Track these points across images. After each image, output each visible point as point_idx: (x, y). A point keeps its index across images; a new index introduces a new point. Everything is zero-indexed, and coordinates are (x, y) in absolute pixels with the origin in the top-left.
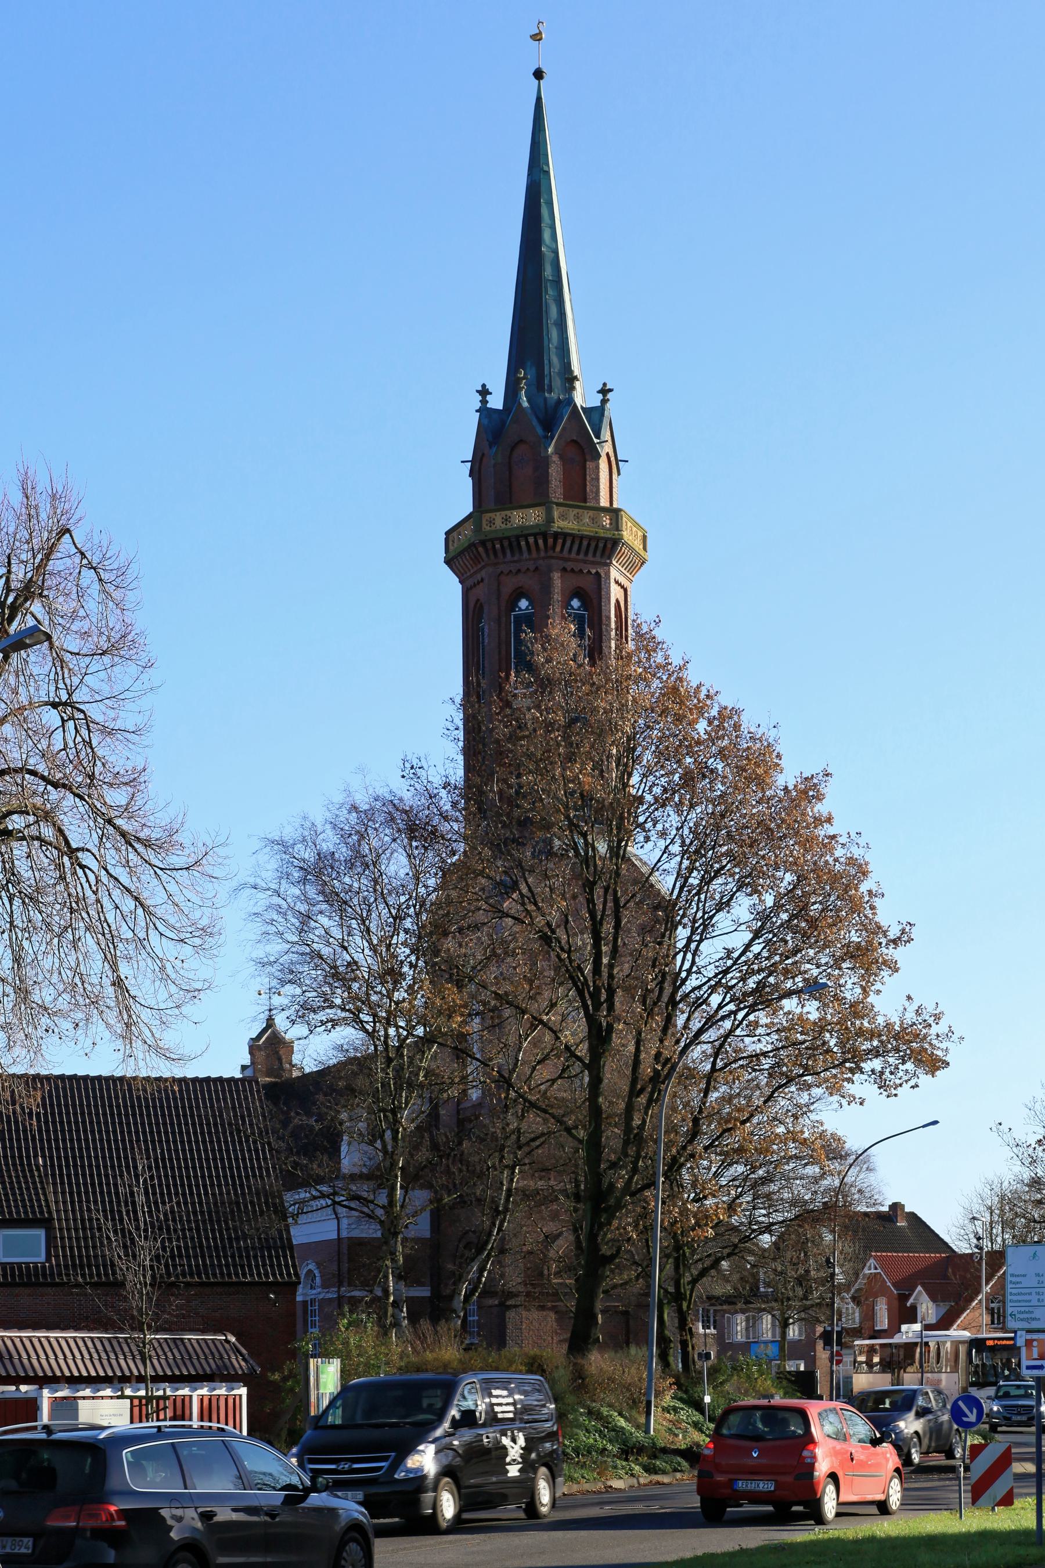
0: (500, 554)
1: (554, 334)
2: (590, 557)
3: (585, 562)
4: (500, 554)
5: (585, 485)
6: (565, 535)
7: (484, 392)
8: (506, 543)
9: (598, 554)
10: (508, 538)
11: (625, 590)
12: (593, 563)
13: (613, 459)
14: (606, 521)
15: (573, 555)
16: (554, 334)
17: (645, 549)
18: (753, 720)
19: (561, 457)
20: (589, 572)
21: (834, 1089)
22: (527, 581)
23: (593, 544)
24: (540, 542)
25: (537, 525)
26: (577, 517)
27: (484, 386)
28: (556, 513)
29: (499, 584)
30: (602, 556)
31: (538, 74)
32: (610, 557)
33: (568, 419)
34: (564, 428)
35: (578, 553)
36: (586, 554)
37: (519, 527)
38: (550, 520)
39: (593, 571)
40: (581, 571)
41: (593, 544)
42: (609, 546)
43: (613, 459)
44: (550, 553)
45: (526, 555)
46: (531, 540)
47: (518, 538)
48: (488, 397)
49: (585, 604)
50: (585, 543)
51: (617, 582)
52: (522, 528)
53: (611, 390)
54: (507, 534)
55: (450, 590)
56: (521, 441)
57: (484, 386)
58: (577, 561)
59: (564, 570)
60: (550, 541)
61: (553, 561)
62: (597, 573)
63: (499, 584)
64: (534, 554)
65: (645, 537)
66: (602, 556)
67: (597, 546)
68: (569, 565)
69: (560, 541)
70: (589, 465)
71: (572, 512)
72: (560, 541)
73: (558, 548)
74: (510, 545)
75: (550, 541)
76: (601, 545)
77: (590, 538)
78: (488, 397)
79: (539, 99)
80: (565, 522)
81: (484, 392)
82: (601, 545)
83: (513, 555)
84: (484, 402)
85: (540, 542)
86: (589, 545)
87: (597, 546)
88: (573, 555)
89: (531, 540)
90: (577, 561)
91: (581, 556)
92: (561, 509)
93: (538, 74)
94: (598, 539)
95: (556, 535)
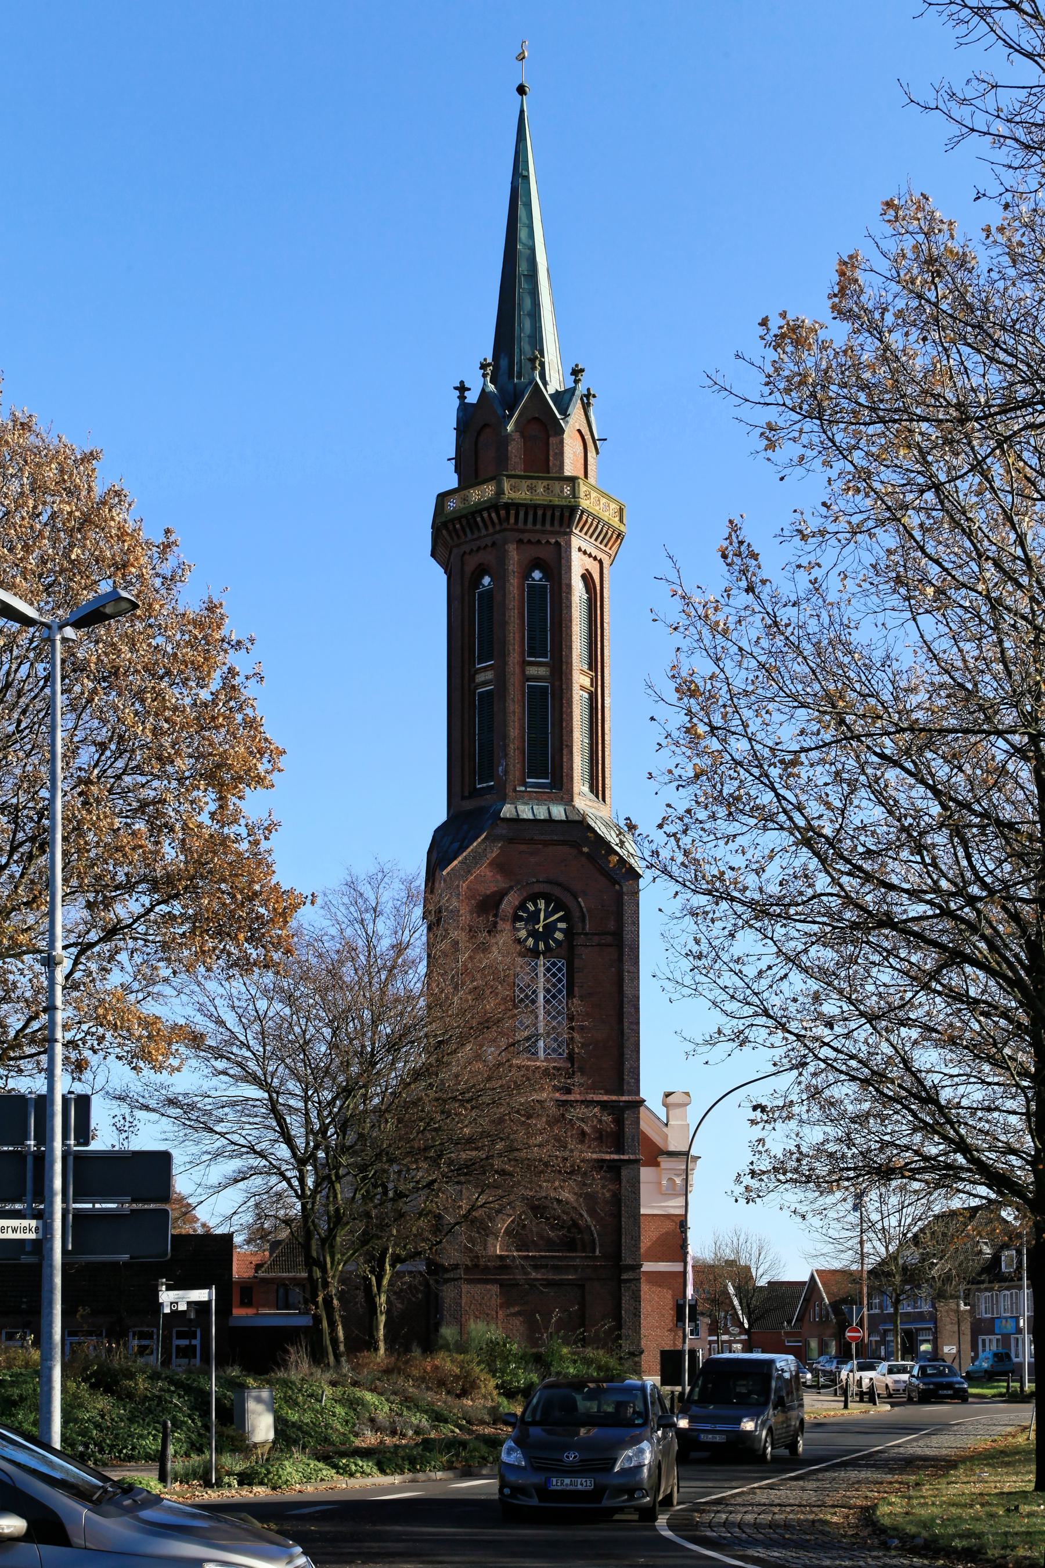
0: (461, 534)
1: (527, 324)
2: (548, 527)
3: (543, 532)
4: (461, 534)
5: (548, 460)
6: (516, 506)
7: (462, 389)
8: (464, 522)
9: (556, 523)
10: (465, 516)
11: (601, 562)
12: (552, 533)
13: (588, 437)
14: (567, 490)
15: (530, 526)
16: (527, 324)
17: (621, 521)
18: (143, 516)
19: (523, 436)
20: (548, 542)
21: (249, 1227)
22: (488, 557)
23: (549, 514)
24: (493, 515)
25: (490, 499)
26: (531, 489)
27: (462, 382)
28: (506, 486)
29: (463, 564)
30: (561, 525)
31: (521, 90)
32: (570, 526)
33: (530, 397)
34: (524, 406)
35: (535, 523)
36: (543, 523)
37: (476, 504)
38: (500, 492)
39: (553, 541)
40: (539, 542)
41: (549, 514)
42: (567, 514)
43: (588, 437)
44: (505, 525)
45: (484, 532)
46: (485, 515)
47: (473, 514)
48: (467, 394)
49: (547, 575)
50: (540, 513)
51: (580, 550)
52: (479, 503)
53: (582, 370)
54: (465, 512)
55: (437, 579)
56: (486, 425)
57: (462, 382)
58: (536, 531)
59: (520, 542)
60: (503, 513)
61: (508, 533)
62: (557, 543)
63: (463, 564)
64: (491, 530)
65: (621, 510)
66: (561, 525)
67: (553, 515)
68: (526, 537)
69: (513, 512)
70: (553, 440)
71: (525, 484)
72: (513, 512)
73: (512, 520)
74: (468, 522)
75: (503, 513)
76: (557, 514)
77: (545, 507)
78: (467, 394)
79: (522, 112)
80: (516, 492)
81: (462, 389)
82: (557, 514)
83: (472, 533)
84: (462, 397)
85: (493, 515)
86: (544, 515)
87: (553, 515)
88: (530, 526)
89: (485, 515)
90: (536, 531)
91: (538, 527)
92: (513, 481)
93: (521, 90)
94: (553, 507)
95: (508, 506)
